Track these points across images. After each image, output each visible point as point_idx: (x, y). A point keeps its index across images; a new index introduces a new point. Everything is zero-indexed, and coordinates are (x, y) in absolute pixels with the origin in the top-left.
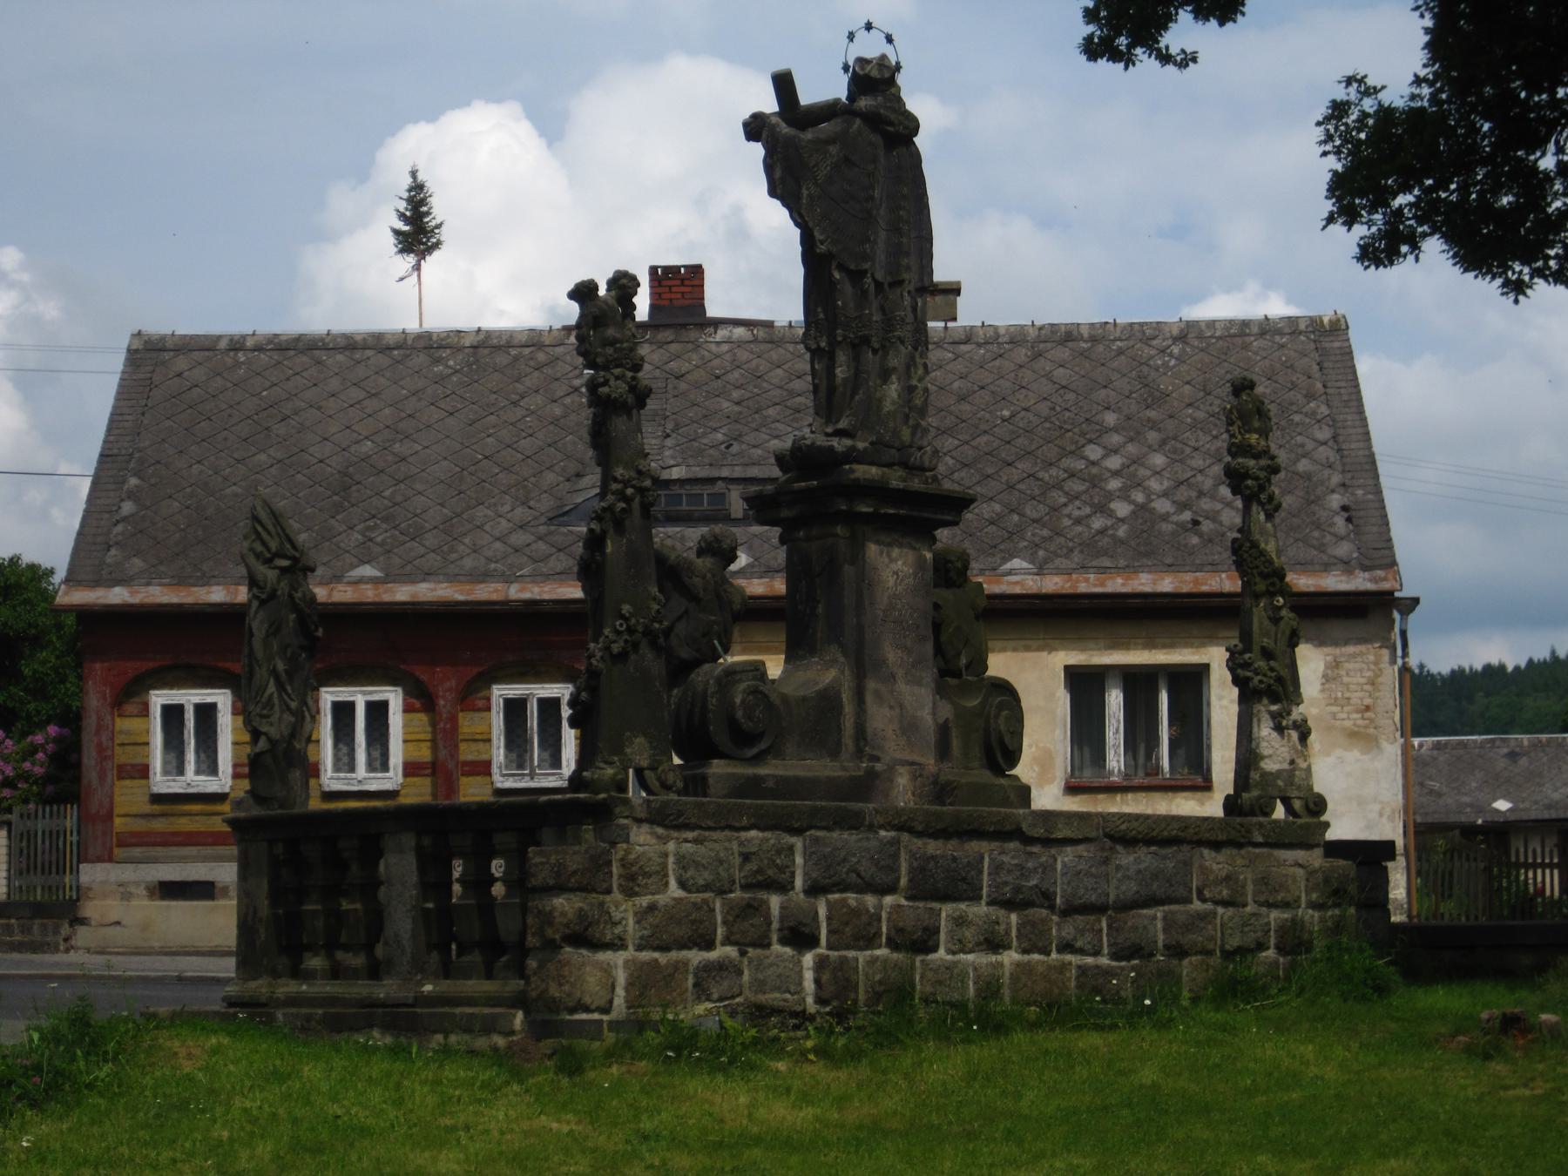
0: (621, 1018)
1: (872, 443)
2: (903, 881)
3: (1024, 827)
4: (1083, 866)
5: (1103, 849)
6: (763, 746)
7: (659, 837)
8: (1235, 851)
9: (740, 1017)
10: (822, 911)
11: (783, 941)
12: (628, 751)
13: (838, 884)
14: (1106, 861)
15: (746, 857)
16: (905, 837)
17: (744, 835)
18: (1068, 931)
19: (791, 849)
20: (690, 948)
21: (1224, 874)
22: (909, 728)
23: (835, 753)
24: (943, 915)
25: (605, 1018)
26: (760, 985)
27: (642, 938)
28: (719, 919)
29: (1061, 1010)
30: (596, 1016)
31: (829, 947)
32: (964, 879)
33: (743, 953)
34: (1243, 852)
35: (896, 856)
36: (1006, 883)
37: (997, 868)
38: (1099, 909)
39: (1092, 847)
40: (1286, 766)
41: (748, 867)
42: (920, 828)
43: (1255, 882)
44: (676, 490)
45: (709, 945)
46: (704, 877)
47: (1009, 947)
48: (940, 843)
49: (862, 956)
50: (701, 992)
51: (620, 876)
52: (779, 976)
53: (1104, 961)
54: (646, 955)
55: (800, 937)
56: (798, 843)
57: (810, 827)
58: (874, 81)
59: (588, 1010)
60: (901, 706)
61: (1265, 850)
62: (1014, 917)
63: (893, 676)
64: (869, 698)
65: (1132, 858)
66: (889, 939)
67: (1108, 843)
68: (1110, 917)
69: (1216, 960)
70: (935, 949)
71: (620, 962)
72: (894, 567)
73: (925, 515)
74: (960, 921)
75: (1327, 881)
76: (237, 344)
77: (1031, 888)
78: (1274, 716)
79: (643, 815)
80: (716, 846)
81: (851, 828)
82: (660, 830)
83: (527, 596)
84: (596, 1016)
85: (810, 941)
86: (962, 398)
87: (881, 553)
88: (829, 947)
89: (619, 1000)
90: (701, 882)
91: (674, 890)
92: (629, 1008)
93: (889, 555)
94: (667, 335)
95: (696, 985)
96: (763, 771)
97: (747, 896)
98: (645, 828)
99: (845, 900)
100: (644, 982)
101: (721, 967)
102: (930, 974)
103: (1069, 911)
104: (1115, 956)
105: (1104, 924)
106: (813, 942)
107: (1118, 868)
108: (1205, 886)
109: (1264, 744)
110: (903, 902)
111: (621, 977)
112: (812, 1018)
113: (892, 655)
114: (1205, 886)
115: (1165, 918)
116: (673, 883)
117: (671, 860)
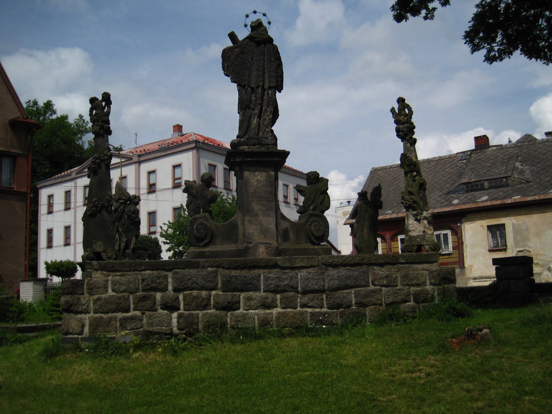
0: (86, 337)
1: (247, 139)
2: (220, 285)
3: (279, 263)
4: (311, 276)
5: (321, 269)
6: (206, 241)
7: (104, 275)
8: (391, 266)
9: (140, 336)
10: (181, 297)
11: (163, 309)
12: (94, 246)
13: (188, 288)
14: (322, 274)
15: (143, 280)
16: (221, 269)
17: (143, 272)
18: (306, 299)
19: (166, 277)
20: (118, 312)
21: (384, 275)
22: (264, 232)
23: (236, 242)
24: (242, 296)
25: (80, 337)
26: (151, 324)
27: (95, 309)
28: (132, 302)
29: (299, 329)
30: (76, 336)
31: (185, 310)
32: (250, 284)
33: (143, 314)
34: (395, 266)
35: (216, 276)
36: (271, 284)
37: (266, 279)
38: (323, 291)
39: (316, 269)
40: (421, 233)
41: (145, 283)
42: (227, 266)
43: (401, 277)
44: (473, 184)
45: (128, 311)
46: (124, 287)
47: (277, 307)
48: (239, 271)
49: (201, 313)
50: (123, 326)
51: (87, 289)
52: (160, 321)
53: (325, 310)
54: (98, 315)
55: (171, 307)
56: (170, 274)
57: (174, 269)
58: (257, 27)
59: (72, 334)
60: (261, 224)
61: (407, 265)
62: (278, 296)
63: (258, 215)
64: (246, 222)
65: (336, 272)
66: (214, 306)
67: (324, 267)
68: (327, 294)
69: (383, 307)
70: (238, 308)
71: (87, 318)
72: (257, 178)
73: (264, 159)
74: (249, 299)
75: (438, 275)
76: (391, 167)
77: (285, 285)
78: (414, 215)
79: (98, 268)
80: (129, 277)
81: (194, 268)
82: (105, 273)
83: (437, 211)
84: (76, 336)
85: (175, 308)
86: (544, 154)
87: (251, 174)
88: (185, 310)
89: (86, 329)
90: (122, 289)
91: (110, 292)
92: (90, 333)
93: (254, 174)
94: (479, 151)
95: (120, 325)
96: (205, 250)
97: (144, 293)
98: (99, 272)
99: (192, 293)
100: (95, 325)
101: (132, 318)
102: (234, 318)
103: (305, 293)
104: (329, 308)
105: (324, 296)
106: (178, 309)
107: (328, 276)
108: (375, 280)
109: (410, 226)
110: (221, 293)
111: (87, 323)
112: (176, 335)
113: (256, 207)
114: (375, 280)
115: (355, 293)
116: (110, 290)
117: (110, 282)
